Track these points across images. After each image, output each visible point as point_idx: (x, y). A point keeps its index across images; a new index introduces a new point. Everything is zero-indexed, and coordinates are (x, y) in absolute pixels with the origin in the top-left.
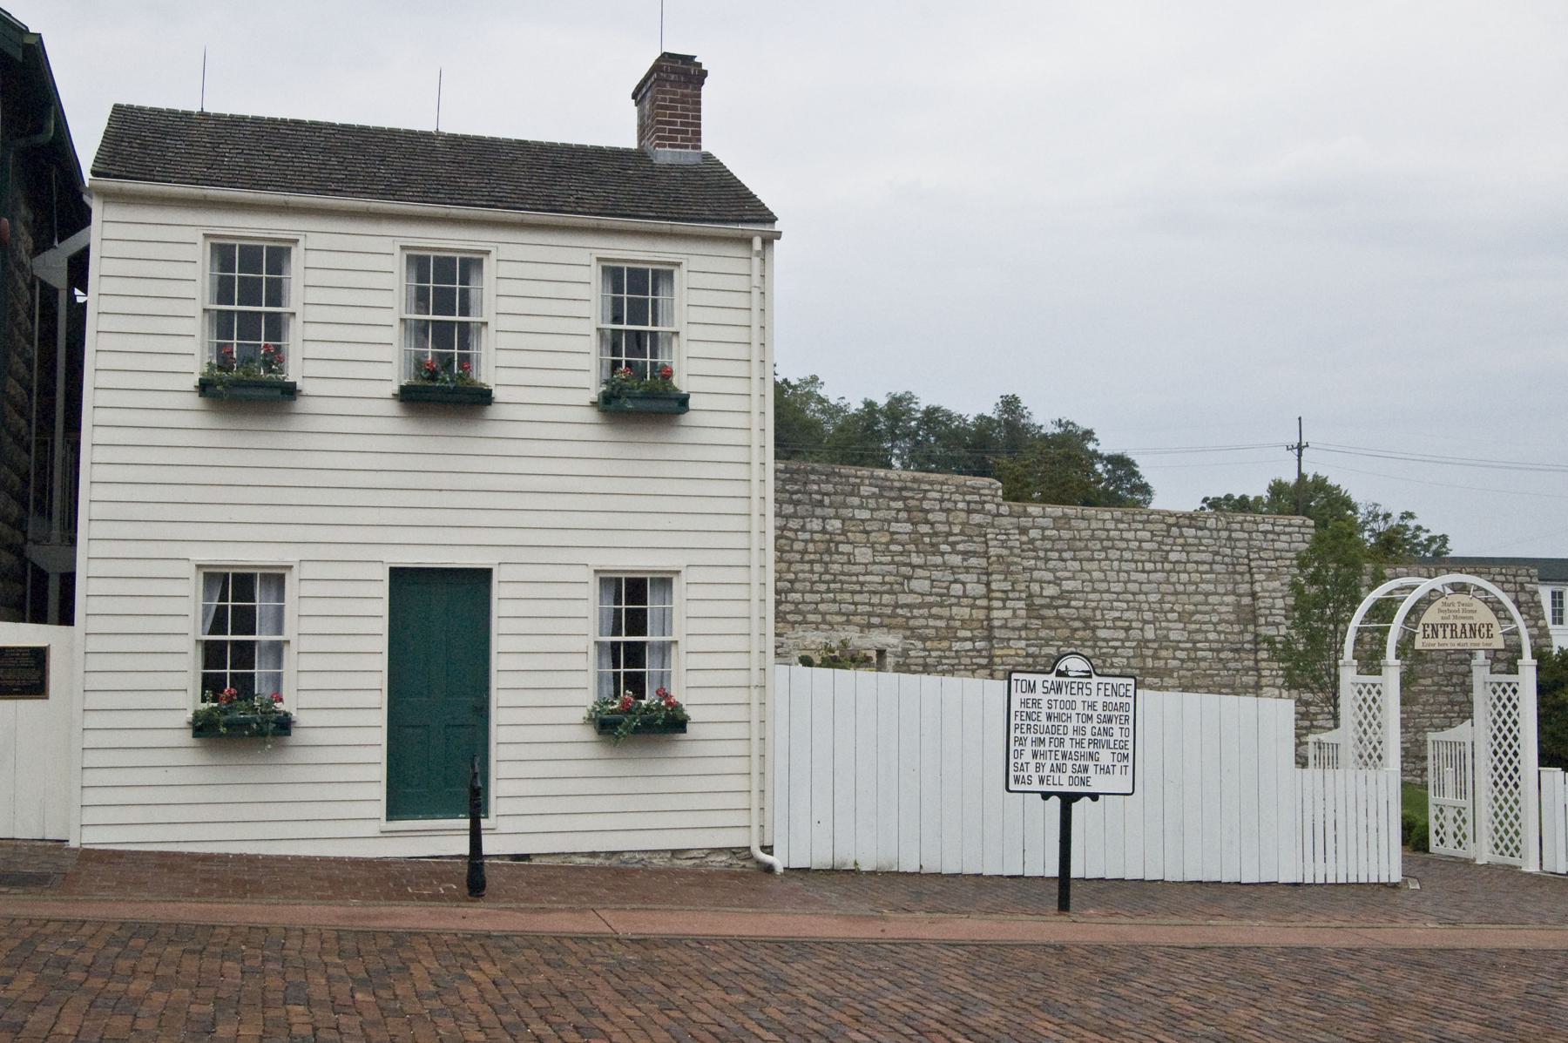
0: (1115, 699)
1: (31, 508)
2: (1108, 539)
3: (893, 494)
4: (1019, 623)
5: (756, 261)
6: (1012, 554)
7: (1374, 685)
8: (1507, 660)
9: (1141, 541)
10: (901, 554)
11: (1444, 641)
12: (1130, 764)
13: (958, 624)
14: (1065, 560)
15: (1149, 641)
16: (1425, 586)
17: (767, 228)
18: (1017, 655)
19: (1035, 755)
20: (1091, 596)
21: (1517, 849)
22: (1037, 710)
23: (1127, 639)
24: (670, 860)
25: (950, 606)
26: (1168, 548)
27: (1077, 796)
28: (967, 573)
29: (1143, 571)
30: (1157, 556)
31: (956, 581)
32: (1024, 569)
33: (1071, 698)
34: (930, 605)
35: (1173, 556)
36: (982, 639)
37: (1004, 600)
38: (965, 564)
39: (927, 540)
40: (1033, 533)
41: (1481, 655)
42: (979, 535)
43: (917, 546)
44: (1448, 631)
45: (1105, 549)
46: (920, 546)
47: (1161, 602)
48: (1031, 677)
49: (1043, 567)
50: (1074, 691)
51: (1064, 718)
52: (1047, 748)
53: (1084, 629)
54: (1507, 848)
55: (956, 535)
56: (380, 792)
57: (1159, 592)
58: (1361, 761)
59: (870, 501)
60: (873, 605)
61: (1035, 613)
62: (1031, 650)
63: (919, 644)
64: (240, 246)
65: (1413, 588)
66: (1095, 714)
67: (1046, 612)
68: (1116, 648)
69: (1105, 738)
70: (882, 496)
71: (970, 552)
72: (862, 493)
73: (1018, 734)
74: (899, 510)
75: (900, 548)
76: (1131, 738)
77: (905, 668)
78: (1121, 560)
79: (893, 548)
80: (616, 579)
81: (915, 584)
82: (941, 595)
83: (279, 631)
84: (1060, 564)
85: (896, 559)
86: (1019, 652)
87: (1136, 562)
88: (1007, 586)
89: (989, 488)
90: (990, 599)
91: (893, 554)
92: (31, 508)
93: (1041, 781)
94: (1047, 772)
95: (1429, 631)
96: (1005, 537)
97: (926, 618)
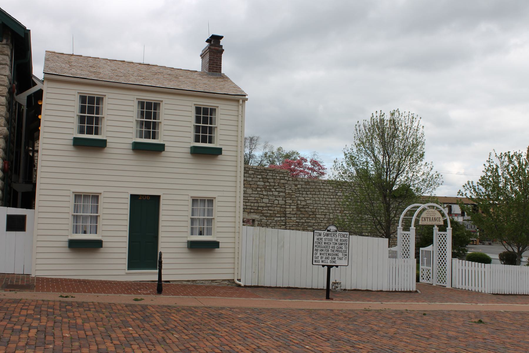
0: (343, 238)
1: (13, 172)
2: (320, 188)
3: (258, 173)
4: (294, 213)
5: (240, 107)
6: (292, 192)
7: (407, 234)
8: (443, 228)
9: (329, 189)
10: (260, 191)
11: (427, 222)
12: (347, 257)
13: (276, 212)
14: (308, 194)
15: (331, 219)
16: (422, 206)
17: (244, 97)
18: (293, 222)
19: (320, 254)
20: (315, 205)
21: (445, 281)
22: (321, 241)
23: (325, 218)
24: (211, 283)
25: (274, 207)
26: (337, 191)
27: (332, 266)
28: (280, 197)
29: (330, 198)
30: (334, 194)
31: (276, 200)
32: (296, 197)
33: (331, 238)
34: (268, 207)
35: (339, 194)
36: (283, 217)
37: (290, 206)
38: (279, 195)
39: (268, 187)
40: (299, 186)
41: (436, 227)
42: (284, 186)
43: (265, 189)
44: (428, 219)
45: (319, 191)
46: (266, 189)
47: (335, 207)
48: (320, 232)
49: (301, 196)
50: (332, 236)
51: (329, 243)
52: (324, 252)
53: (313, 215)
54: (442, 281)
55: (276, 186)
56: (126, 261)
57: (334, 204)
58: (403, 256)
59: (252, 175)
60: (252, 206)
61: (299, 210)
62: (297, 220)
63: (265, 218)
64: (97, 97)
65: (418, 207)
66: (338, 243)
67: (302, 209)
68: (322, 220)
69: (340, 249)
70: (255, 174)
71: (280, 191)
72: (249, 173)
73: (316, 248)
74: (260, 178)
75: (260, 190)
76: (348, 250)
77: (261, 225)
78: (324, 195)
79: (258, 189)
80: (204, 199)
81: (264, 200)
82: (271, 204)
83: (97, 213)
84: (307, 196)
85: (259, 193)
86: (294, 221)
87: (328, 195)
88: (291, 201)
89: (286, 173)
90: (286, 205)
91: (258, 191)
92: (13, 172)
93: (322, 262)
94: (324, 259)
95: (423, 219)
96: (291, 187)
97: (267, 210)
